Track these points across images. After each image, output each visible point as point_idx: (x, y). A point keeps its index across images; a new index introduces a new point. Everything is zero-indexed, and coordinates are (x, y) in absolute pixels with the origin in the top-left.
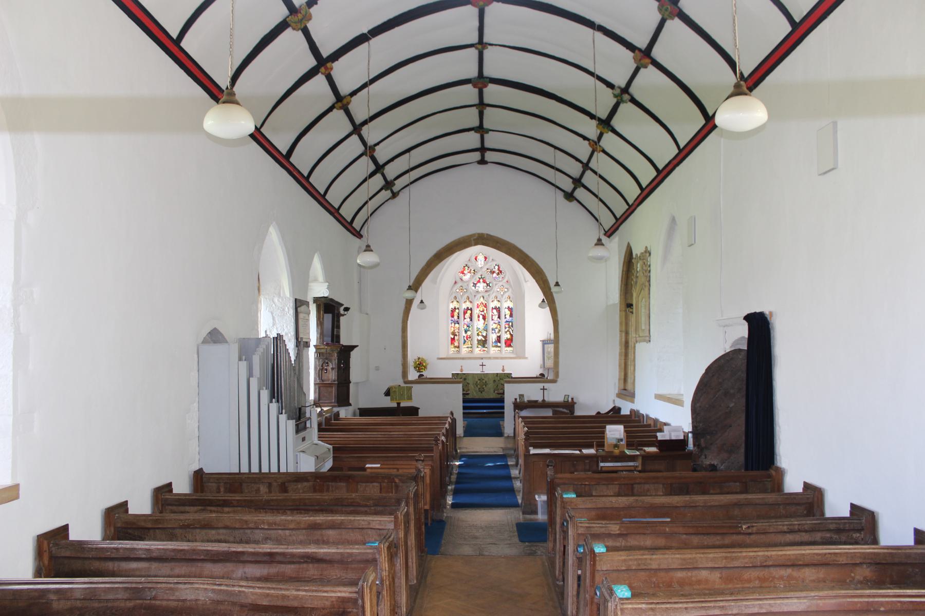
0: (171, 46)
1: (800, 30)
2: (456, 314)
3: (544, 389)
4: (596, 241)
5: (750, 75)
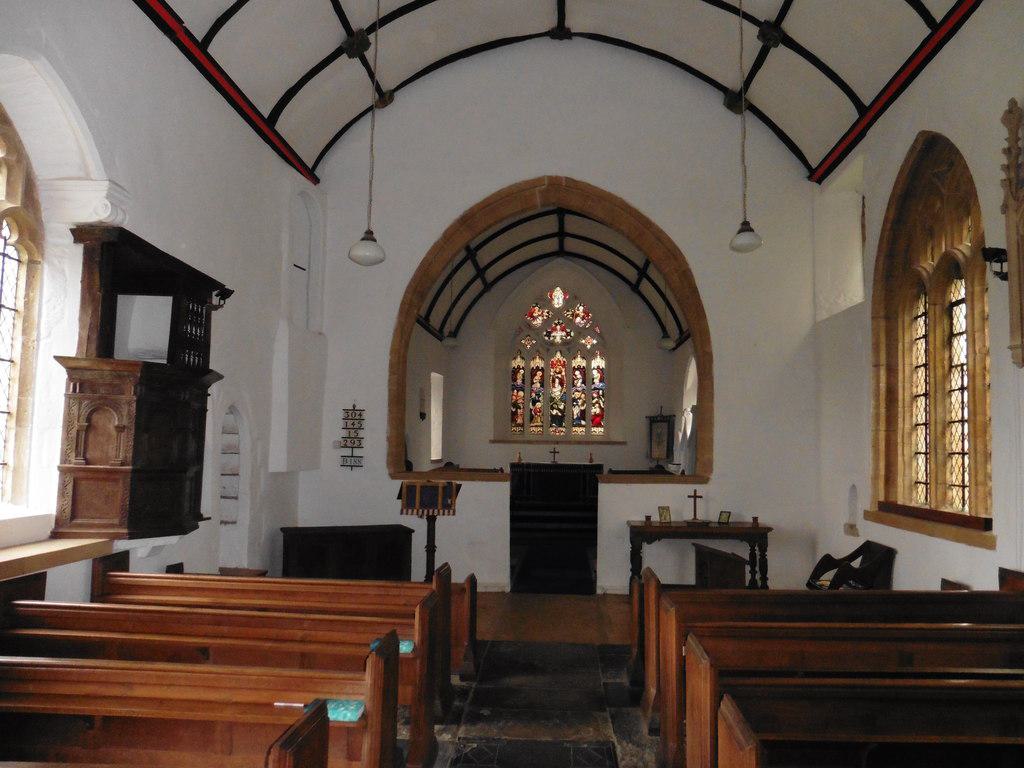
0: (196, 51)
1: (941, 33)
2: (519, 377)
3: (695, 497)
4: (739, 227)
5: (819, 166)
